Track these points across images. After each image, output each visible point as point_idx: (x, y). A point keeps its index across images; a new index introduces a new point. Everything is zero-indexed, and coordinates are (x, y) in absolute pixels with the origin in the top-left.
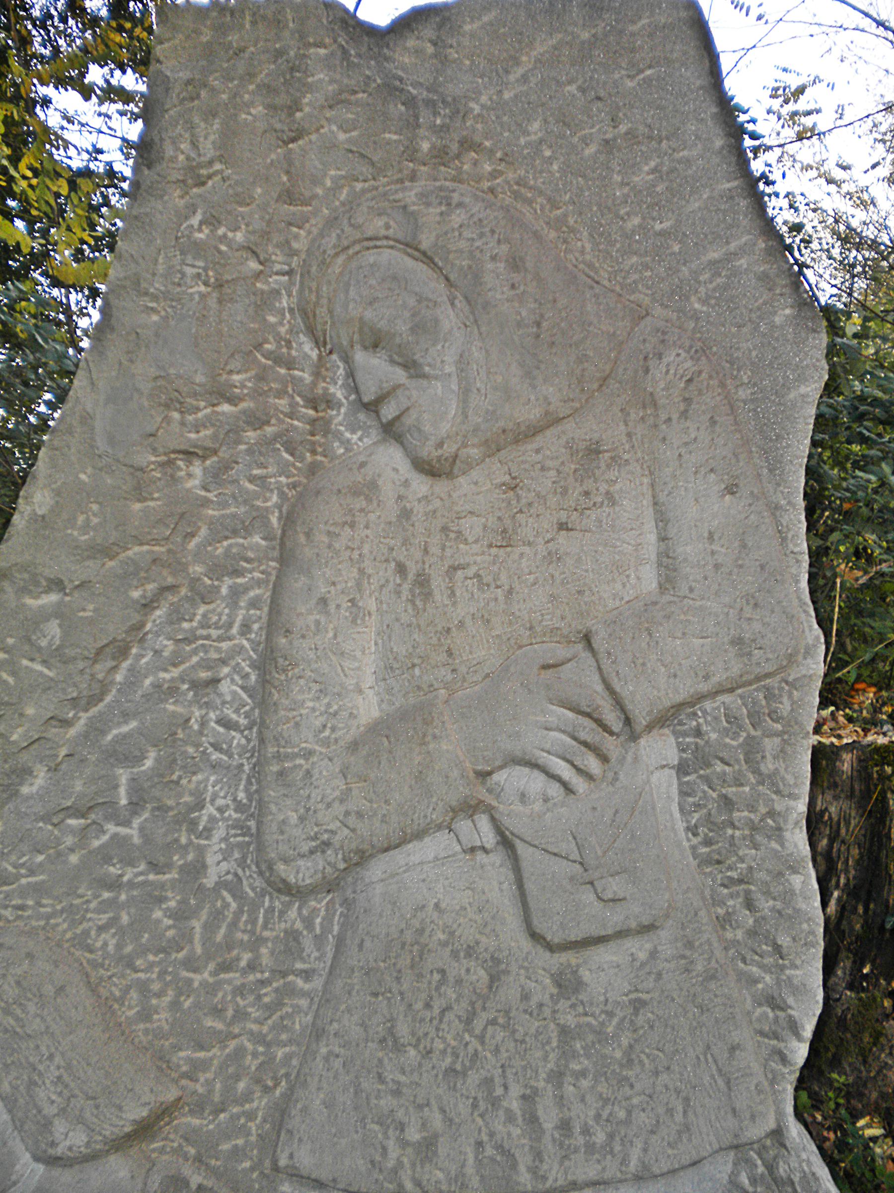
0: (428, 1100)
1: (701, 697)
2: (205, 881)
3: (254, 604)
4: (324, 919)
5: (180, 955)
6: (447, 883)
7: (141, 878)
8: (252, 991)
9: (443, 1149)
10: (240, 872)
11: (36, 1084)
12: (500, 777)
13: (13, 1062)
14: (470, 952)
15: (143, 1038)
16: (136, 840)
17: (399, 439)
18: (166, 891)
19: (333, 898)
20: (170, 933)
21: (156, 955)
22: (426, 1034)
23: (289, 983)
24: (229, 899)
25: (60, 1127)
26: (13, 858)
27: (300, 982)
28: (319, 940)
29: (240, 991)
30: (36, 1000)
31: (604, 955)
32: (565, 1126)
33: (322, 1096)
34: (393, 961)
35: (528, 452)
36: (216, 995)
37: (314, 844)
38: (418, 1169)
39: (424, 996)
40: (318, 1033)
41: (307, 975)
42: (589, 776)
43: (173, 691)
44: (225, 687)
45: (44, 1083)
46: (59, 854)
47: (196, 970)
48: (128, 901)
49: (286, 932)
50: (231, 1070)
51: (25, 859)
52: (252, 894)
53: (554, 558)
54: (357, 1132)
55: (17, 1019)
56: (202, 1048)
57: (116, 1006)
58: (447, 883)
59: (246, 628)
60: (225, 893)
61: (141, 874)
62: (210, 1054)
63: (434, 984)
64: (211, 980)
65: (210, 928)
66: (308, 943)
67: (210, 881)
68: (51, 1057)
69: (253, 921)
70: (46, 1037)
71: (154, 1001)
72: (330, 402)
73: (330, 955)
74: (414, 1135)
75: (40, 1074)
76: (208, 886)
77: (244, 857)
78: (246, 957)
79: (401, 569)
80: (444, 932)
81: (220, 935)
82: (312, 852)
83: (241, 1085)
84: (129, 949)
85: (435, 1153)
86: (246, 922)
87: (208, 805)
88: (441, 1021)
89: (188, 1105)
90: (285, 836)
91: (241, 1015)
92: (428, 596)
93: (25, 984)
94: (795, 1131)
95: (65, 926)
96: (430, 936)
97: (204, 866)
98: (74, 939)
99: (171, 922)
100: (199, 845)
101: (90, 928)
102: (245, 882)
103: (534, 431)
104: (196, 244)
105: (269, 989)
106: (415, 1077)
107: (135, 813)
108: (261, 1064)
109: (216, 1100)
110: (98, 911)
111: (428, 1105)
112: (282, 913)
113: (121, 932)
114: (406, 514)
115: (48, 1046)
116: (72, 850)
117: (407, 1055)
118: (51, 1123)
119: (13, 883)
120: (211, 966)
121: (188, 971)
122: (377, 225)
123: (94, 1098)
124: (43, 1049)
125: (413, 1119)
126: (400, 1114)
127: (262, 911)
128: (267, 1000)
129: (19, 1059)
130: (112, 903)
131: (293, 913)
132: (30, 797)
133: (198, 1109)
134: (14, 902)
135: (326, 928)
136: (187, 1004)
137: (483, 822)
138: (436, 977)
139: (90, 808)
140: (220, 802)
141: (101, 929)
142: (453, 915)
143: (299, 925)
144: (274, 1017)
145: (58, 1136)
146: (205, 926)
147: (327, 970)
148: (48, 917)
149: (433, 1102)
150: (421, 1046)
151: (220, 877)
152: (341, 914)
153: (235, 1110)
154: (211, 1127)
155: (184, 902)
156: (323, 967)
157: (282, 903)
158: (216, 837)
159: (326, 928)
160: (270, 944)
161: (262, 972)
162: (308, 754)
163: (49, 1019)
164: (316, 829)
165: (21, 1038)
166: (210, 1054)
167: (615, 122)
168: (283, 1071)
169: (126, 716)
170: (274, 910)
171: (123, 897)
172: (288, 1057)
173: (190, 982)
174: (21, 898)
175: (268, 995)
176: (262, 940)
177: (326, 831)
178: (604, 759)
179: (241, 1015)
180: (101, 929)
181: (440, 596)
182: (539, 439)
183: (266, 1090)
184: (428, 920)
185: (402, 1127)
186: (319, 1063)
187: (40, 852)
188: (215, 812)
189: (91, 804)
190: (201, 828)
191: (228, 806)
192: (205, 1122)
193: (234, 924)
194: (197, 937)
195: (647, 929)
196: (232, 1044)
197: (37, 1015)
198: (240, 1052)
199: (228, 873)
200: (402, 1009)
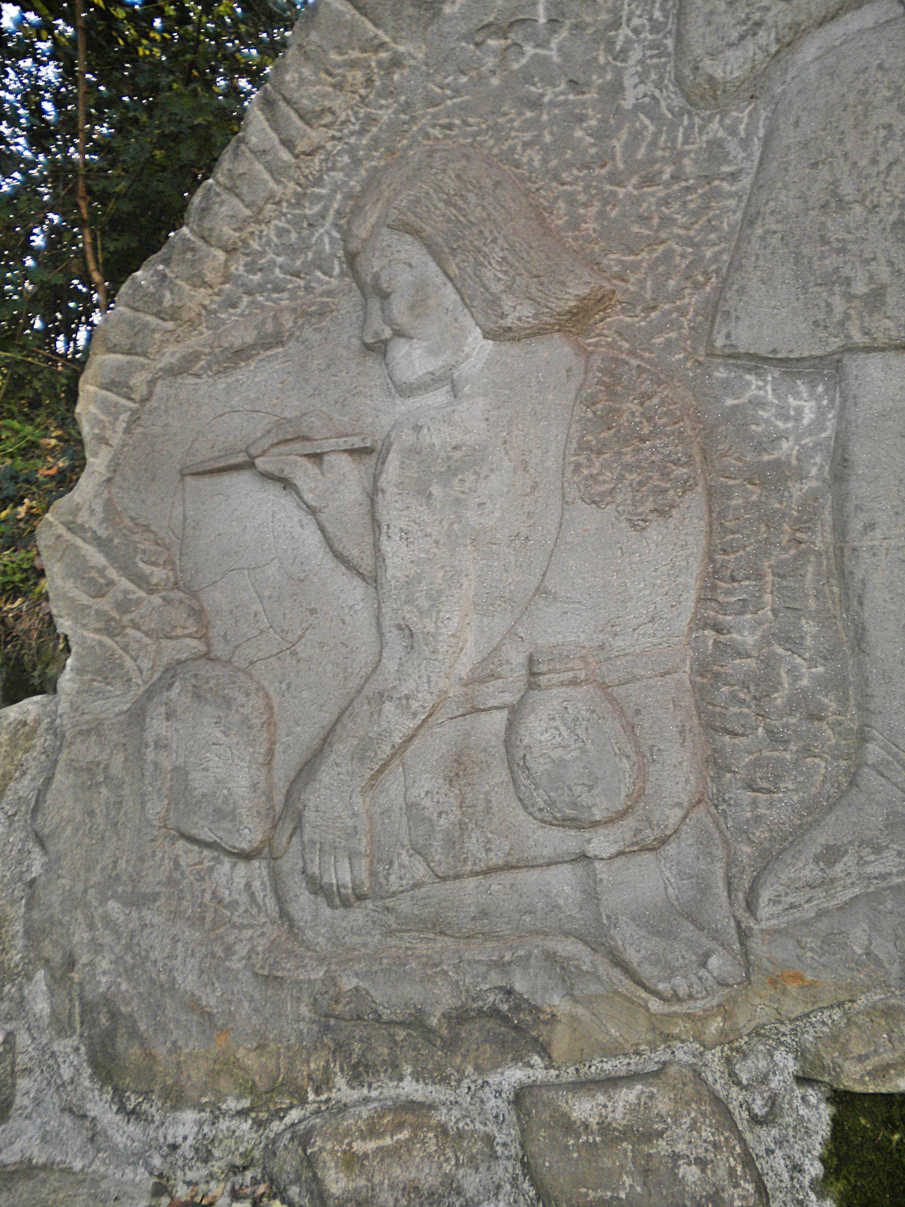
0: (875, 253)
2: (623, 102)
4: (748, 125)
5: (603, 172)
6: (890, 44)
7: (562, 98)
8: (676, 198)
10: (657, 93)
11: (482, 265)
13: (459, 247)
15: (573, 243)
16: (556, 59)
18: (586, 108)
19: (756, 106)
20: (593, 151)
21: (580, 170)
22: (873, 189)
23: (716, 187)
24: (647, 122)
25: (507, 302)
26: (438, 78)
27: (726, 186)
28: (745, 143)
29: (665, 202)
30: (476, 191)
33: (759, 273)
34: (835, 124)
36: (640, 206)
37: (744, 28)
38: (866, 319)
39: (869, 152)
40: (750, 220)
45: (490, 263)
46: (481, 77)
47: (620, 184)
48: (550, 120)
49: (708, 142)
50: (661, 269)
51: (450, 79)
52: (669, 116)
54: (798, 299)
55: (460, 209)
56: (631, 252)
57: (546, 215)
58: (890, 44)
60: (642, 116)
61: (562, 93)
62: (639, 257)
63: (880, 140)
64: (635, 193)
66: (732, 146)
67: (628, 102)
68: (494, 241)
69: (674, 140)
70: (488, 223)
71: (582, 211)
73: (757, 154)
74: (860, 288)
75: (485, 256)
76: (627, 107)
77: (661, 78)
78: (668, 170)
80: (889, 88)
81: (641, 153)
82: (742, 38)
83: (672, 283)
84: (554, 163)
85: (884, 304)
86: (666, 142)
87: (624, 25)
88: (888, 175)
89: (620, 303)
90: (713, 27)
91: (667, 221)
93: (465, 177)
95: (492, 142)
96: (874, 94)
97: (622, 88)
98: (501, 154)
99: (592, 140)
100: (616, 66)
101: (516, 145)
102: (663, 104)
105: (695, 196)
106: (861, 233)
107: (553, 32)
108: (691, 262)
109: (648, 296)
110: (522, 130)
111: (874, 259)
112: (702, 129)
113: (546, 150)
115: (491, 232)
116: (493, 72)
117: (852, 212)
118: (499, 299)
119: (438, 105)
120: (635, 180)
121: (612, 184)
123: (537, 276)
124: (487, 234)
125: (859, 273)
126: (846, 271)
127: (681, 129)
128: (692, 206)
129: (465, 245)
130: (535, 123)
131: (715, 125)
132: (453, 17)
133: (629, 307)
134: (442, 121)
135: (750, 134)
136: (613, 214)
138: (882, 133)
139: (511, 25)
140: (636, 22)
141: (526, 145)
142: (898, 71)
143: (721, 134)
144: (701, 222)
145: (506, 309)
146: (626, 146)
147: (755, 169)
148: (474, 135)
149: (879, 255)
150: (867, 203)
151: (637, 99)
152: (767, 118)
153: (666, 307)
154: (643, 324)
155: (604, 121)
157: (702, 119)
158: (632, 62)
159: (750, 134)
160: (692, 155)
161: (687, 180)
163: (490, 208)
164: (747, 10)
165: (465, 227)
166: (639, 257)
168: (713, 267)
170: (693, 127)
171: (545, 117)
172: (716, 258)
173: (614, 194)
174: (448, 117)
175: (694, 201)
176: (683, 154)
177: (759, 9)
179: (667, 221)
180: (526, 145)
183: (698, 286)
184: (871, 81)
185: (848, 281)
186: (756, 244)
187: (463, 73)
188: (631, 34)
189: (513, 20)
190: (618, 48)
191: (643, 25)
192: (637, 319)
193: (653, 144)
194: (619, 156)
196: (661, 248)
197: (479, 205)
198: (668, 255)
199: (645, 96)
200: (846, 168)
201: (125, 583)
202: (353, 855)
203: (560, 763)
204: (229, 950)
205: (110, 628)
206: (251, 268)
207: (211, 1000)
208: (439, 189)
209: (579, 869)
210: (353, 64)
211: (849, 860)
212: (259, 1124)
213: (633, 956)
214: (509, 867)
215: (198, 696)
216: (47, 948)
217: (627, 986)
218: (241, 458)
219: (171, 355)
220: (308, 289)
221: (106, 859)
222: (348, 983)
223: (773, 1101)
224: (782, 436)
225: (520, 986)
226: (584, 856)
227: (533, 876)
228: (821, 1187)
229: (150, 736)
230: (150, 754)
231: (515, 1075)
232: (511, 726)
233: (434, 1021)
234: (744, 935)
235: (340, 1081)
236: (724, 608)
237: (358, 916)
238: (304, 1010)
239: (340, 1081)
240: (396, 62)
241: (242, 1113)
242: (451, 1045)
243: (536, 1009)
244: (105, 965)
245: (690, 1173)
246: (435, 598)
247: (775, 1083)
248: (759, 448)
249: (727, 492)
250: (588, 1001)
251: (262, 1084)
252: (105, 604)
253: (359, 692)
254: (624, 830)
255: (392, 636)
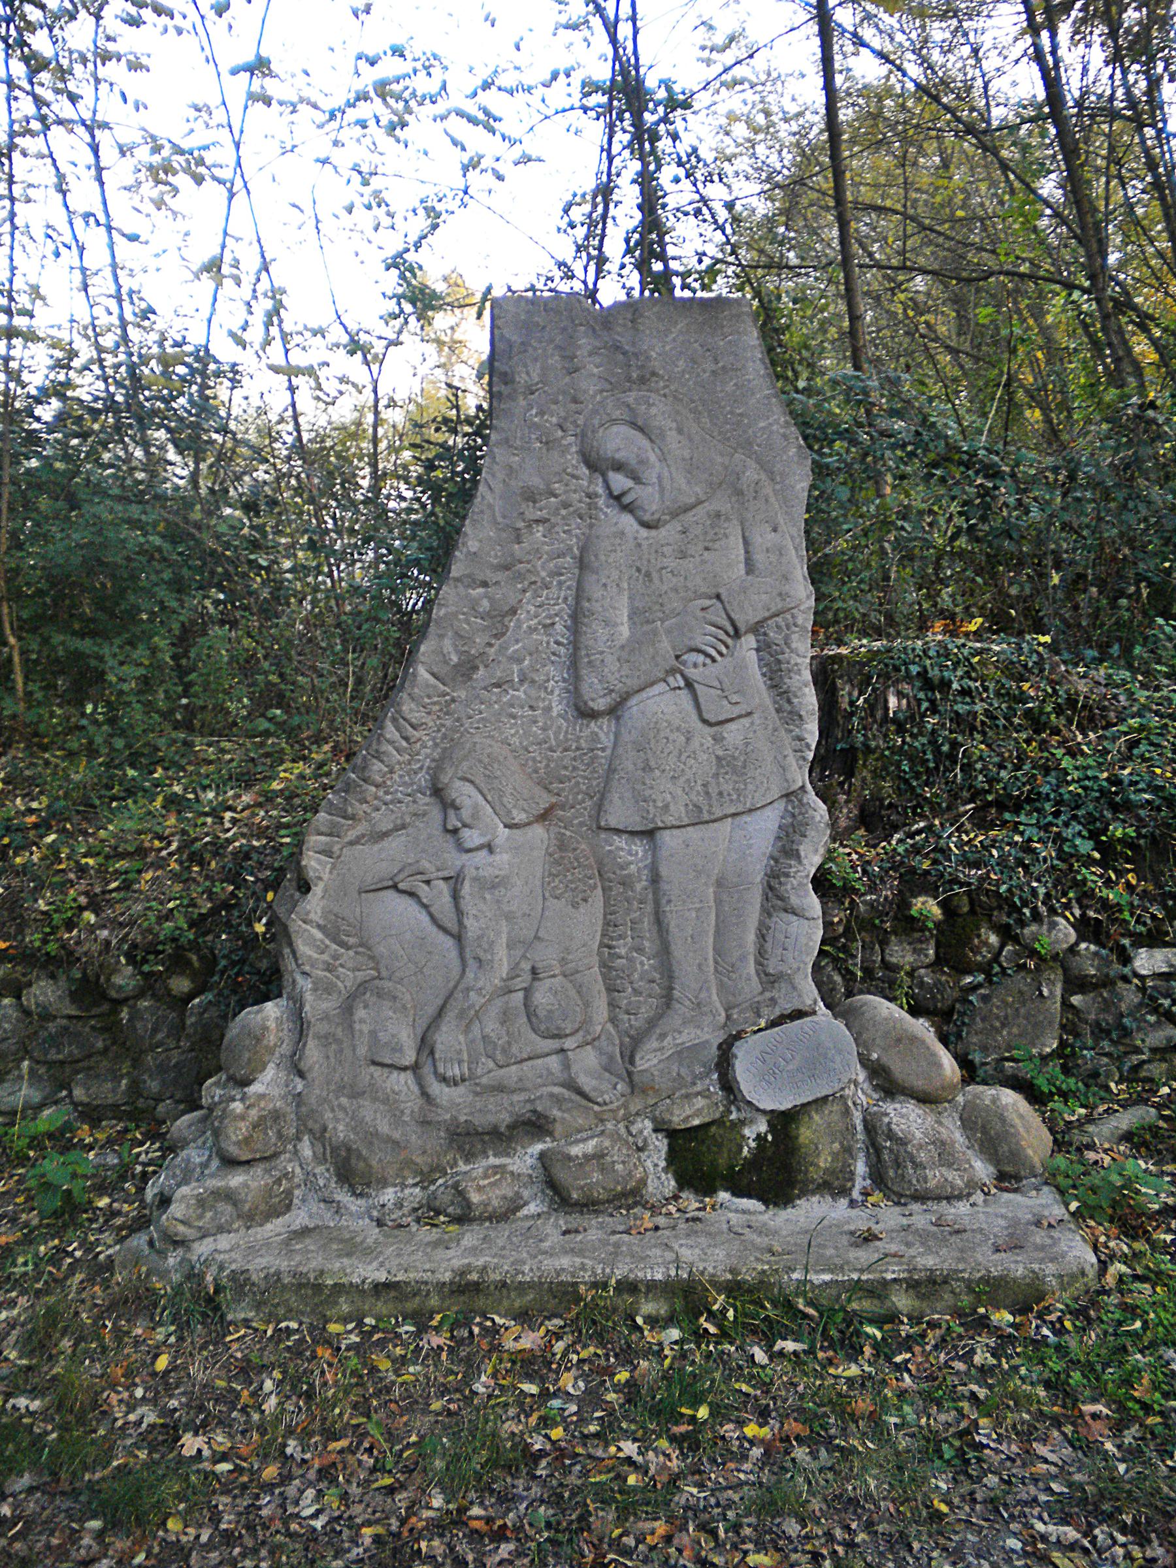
1: (766, 619)
3: (569, 588)
9: (672, 807)
12: (685, 657)
14: (678, 729)
17: (631, 512)
25: (515, 812)
29: (574, 759)
31: (732, 726)
32: (721, 794)
35: (689, 517)
41: (603, 750)
42: (721, 654)
43: (536, 629)
44: (557, 626)
53: (703, 562)
59: (566, 599)
65: (556, 734)
66: (602, 735)
67: (554, 714)
72: (597, 495)
79: (639, 570)
92: (651, 581)
94: (809, 787)
103: (693, 507)
104: (535, 424)
114: (639, 545)
122: (617, 414)
133: (563, 808)
137: (678, 676)
156: (610, 745)
162: (602, 653)
167: (716, 361)
169: (517, 641)
175: (586, 759)
178: (727, 647)
179: (575, 768)
181: (656, 581)
182: (694, 511)
195: (749, 714)
201: (334, 946)
202: (460, 1062)
203: (550, 1011)
204: (402, 1112)
205: (329, 968)
206: (387, 793)
207: (397, 1135)
208: (480, 761)
209: (560, 1056)
210: (434, 703)
211: (669, 1038)
212: (423, 1188)
213: (587, 1089)
214: (530, 1059)
215: (379, 996)
216: (310, 1124)
217: (584, 1102)
218: (390, 883)
219: (351, 835)
220: (414, 802)
221: (337, 1077)
222: (462, 1118)
223: (645, 1140)
224: (631, 863)
225: (539, 1109)
226: (563, 1050)
227: (540, 1061)
228: (665, 1170)
229: (356, 1018)
230: (357, 1026)
231: (539, 1147)
232: (526, 998)
233: (502, 1129)
234: (630, 1074)
235: (461, 1163)
236: (612, 939)
237: (461, 1089)
238: (442, 1134)
239: (461, 1163)
240: (453, 700)
241: (416, 1185)
242: (510, 1139)
243: (546, 1117)
244: (341, 1128)
245: (619, 1167)
246: (492, 944)
247: (645, 1133)
248: (622, 868)
249: (610, 889)
250: (568, 1110)
251: (426, 1169)
252: (325, 957)
253: (455, 987)
254: (579, 1037)
255: (471, 962)
